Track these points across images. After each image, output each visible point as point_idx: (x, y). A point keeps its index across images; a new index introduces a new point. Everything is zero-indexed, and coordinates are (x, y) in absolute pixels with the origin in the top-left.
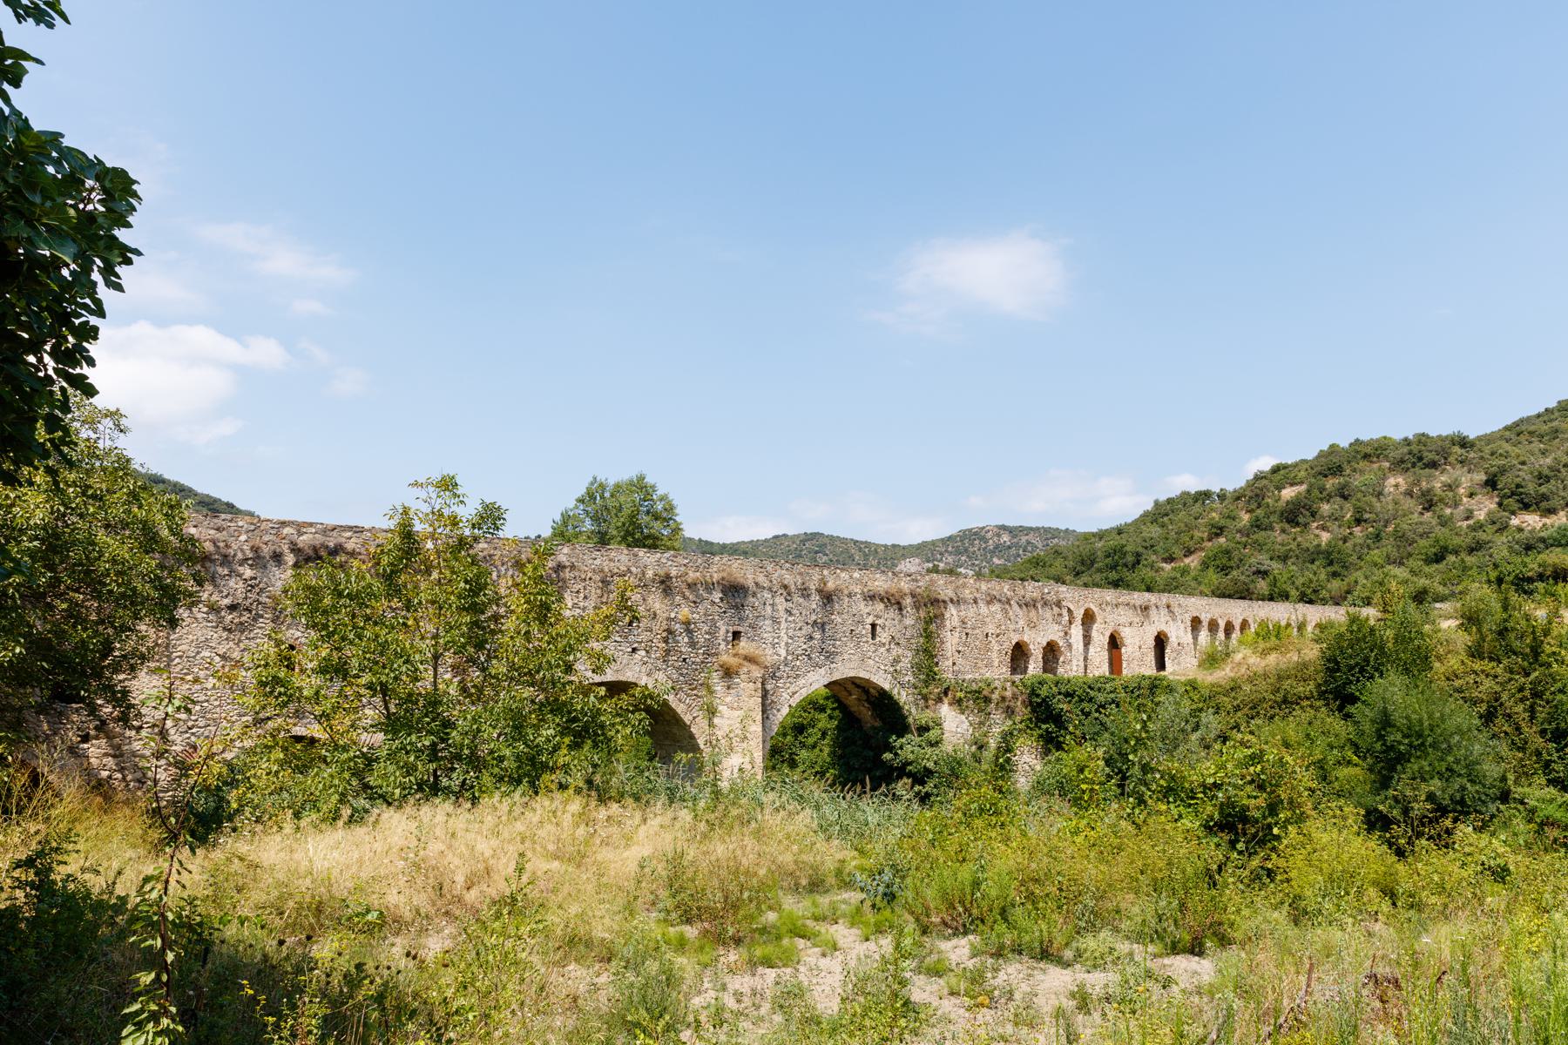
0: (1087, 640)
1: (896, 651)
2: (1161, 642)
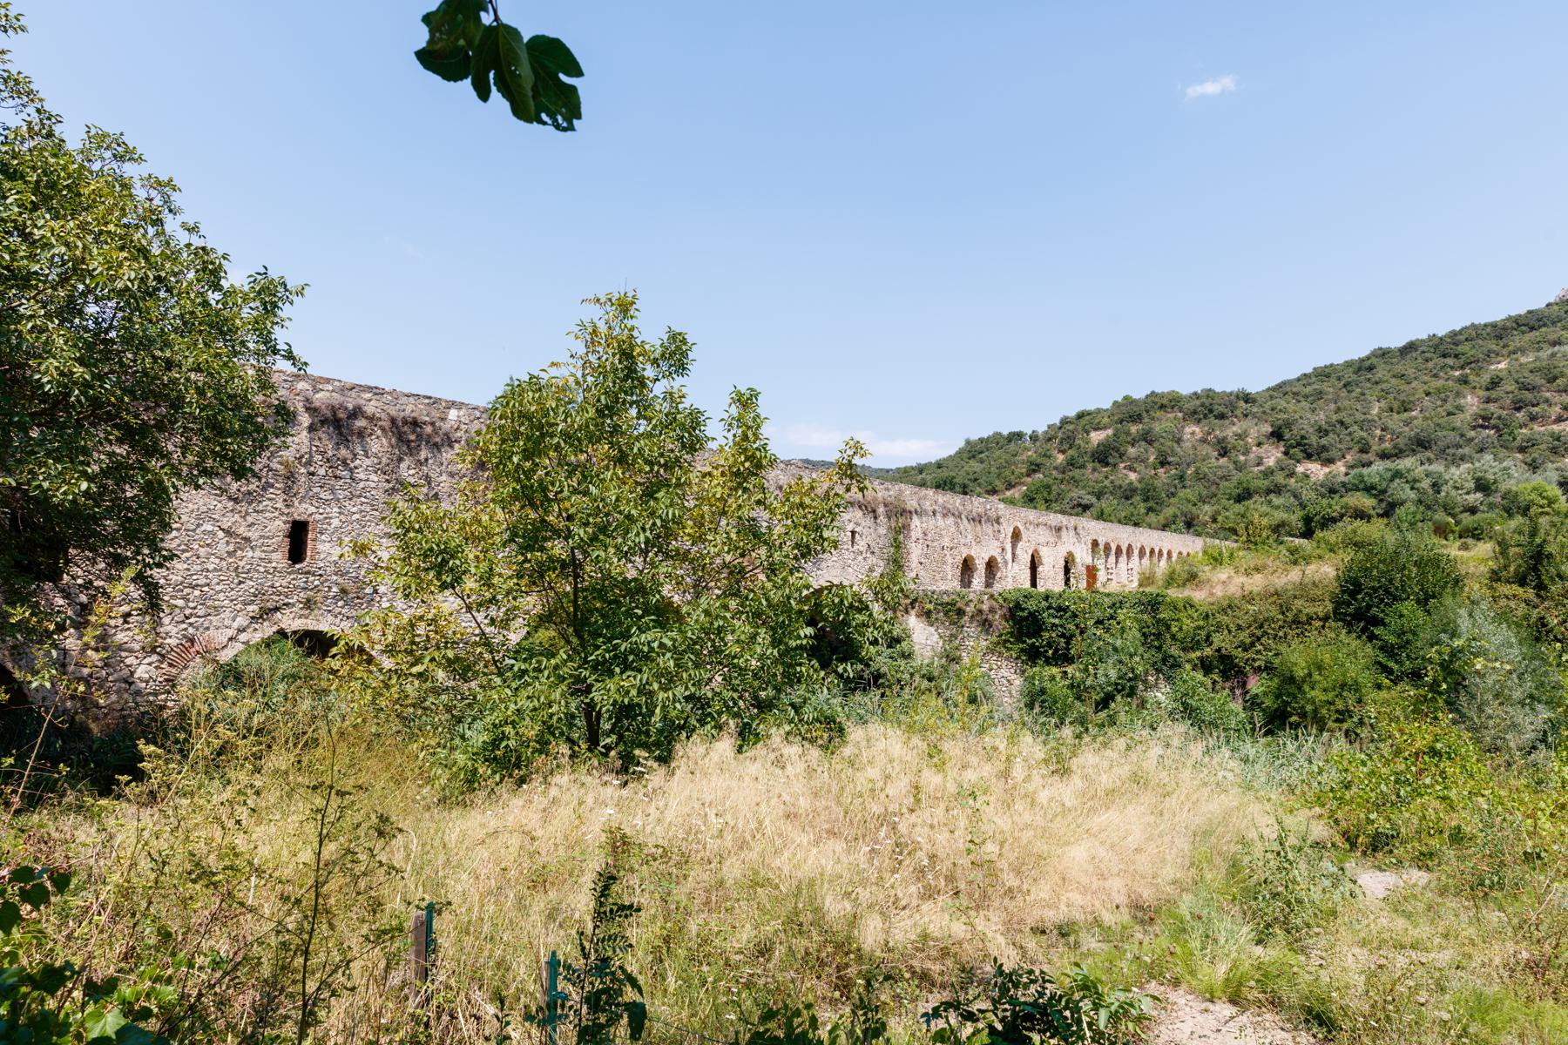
1: (872, 560)
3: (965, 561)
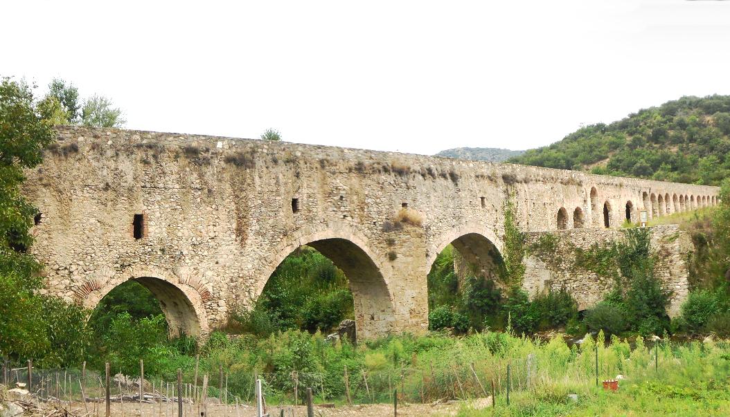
0: (594, 206)
2: (629, 207)
3: (560, 211)
